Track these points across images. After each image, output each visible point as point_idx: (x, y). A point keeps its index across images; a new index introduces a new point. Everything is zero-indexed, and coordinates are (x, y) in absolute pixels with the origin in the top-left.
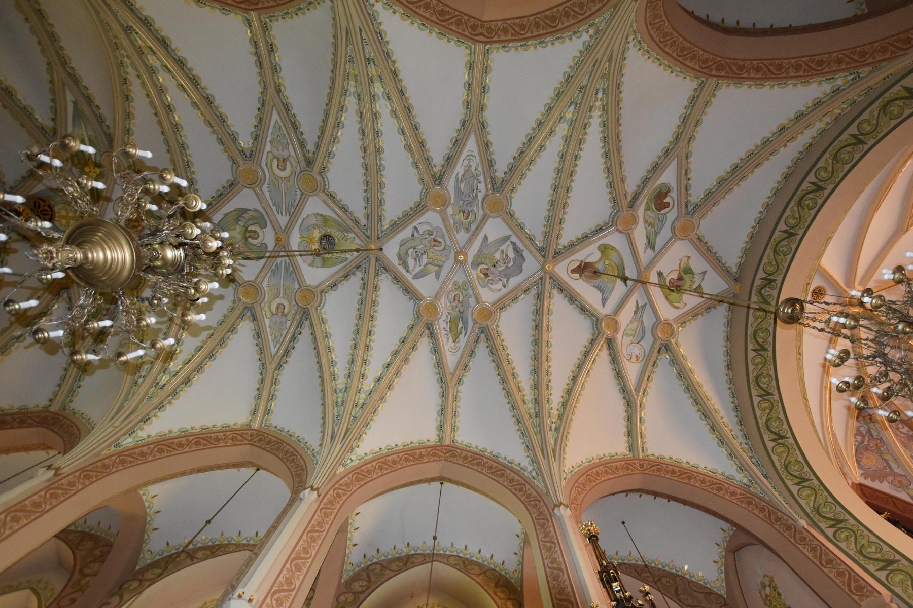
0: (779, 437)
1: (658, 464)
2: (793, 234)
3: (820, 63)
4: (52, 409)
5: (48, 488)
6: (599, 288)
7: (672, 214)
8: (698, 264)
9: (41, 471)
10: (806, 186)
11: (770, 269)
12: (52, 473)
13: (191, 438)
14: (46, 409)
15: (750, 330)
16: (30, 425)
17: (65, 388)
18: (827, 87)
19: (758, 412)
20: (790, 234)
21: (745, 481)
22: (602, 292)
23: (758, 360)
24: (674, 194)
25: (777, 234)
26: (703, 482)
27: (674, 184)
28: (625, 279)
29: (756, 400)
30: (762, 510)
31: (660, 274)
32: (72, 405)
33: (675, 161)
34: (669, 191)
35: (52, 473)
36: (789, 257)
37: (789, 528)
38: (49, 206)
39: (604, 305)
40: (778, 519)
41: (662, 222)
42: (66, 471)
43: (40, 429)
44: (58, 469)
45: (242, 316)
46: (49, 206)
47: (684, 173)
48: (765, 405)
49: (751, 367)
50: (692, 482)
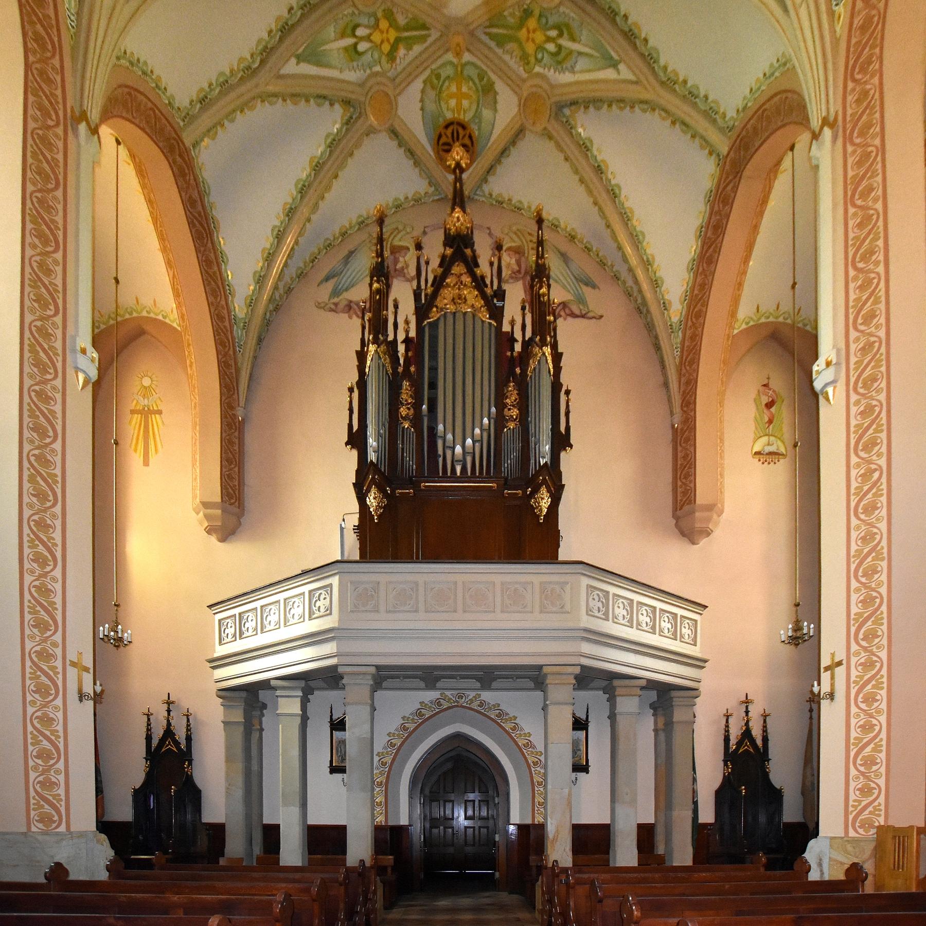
4: (724, 150)
5: (848, 139)
9: (814, 151)
12: (827, 133)
13: (690, 323)
14: (722, 161)
16: (735, 189)
17: (702, 125)
32: (731, 113)
35: (827, 133)
38: (447, 127)
42: (835, 107)
43: (746, 173)
44: (825, 122)
45: (569, 128)
46: (447, 127)
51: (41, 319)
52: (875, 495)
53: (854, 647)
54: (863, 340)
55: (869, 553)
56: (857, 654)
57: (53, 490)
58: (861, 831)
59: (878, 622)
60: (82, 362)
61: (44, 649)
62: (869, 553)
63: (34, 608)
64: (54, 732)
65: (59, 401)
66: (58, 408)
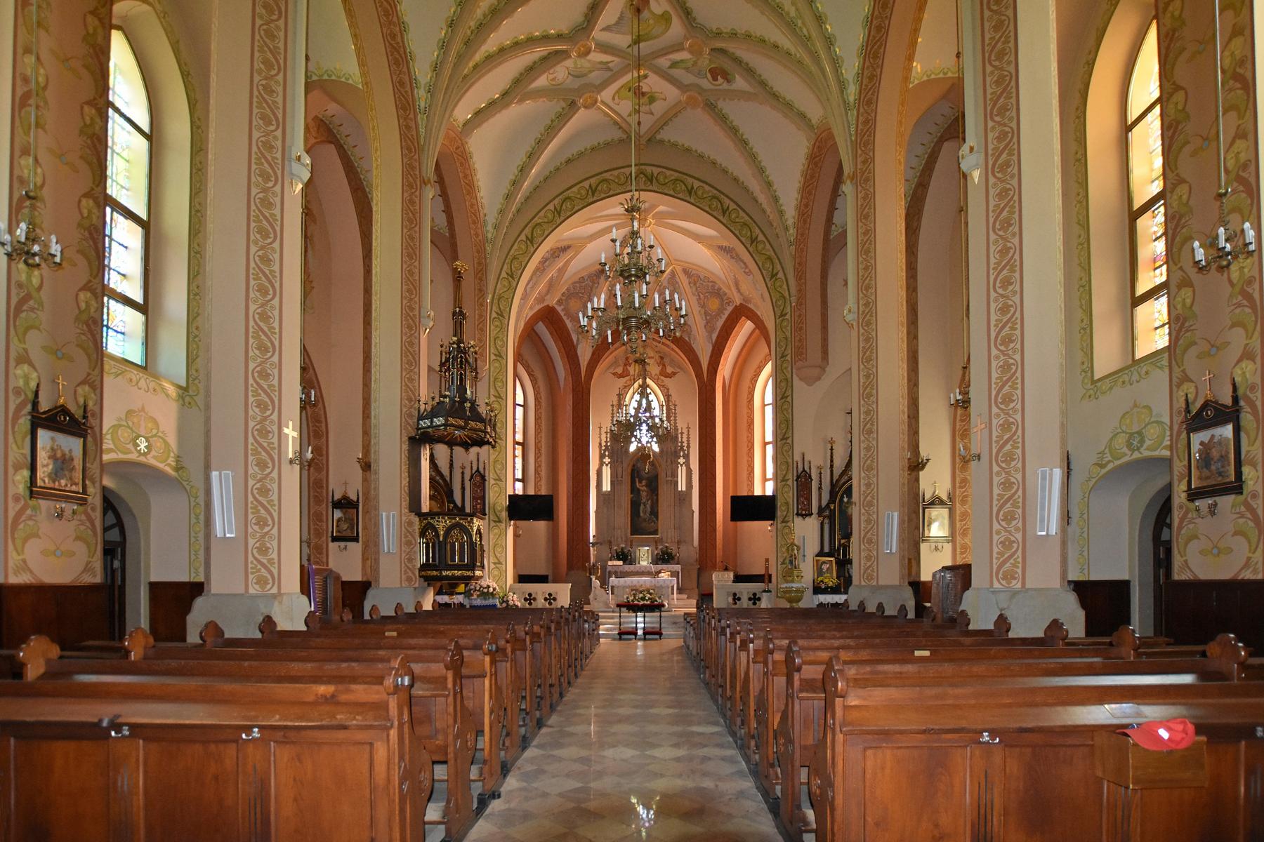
0: (531, 240)
1: (466, 160)
2: (690, 194)
3: (805, 222)
6: (621, 18)
7: (706, 83)
8: (659, 108)
10: (727, 202)
11: (661, 178)
15: (606, 175)
18: (790, 222)
19: (542, 214)
20: (690, 191)
21: (489, 236)
22: (617, 23)
23: (584, 192)
24: (725, 86)
25: (690, 180)
26: (472, 206)
27: (734, 86)
28: (637, 41)
29: (551, 207)
30: (479, 264)
31: (646, 77)
33: (751, 90)
34: (728, 81)
36: (671, 192)
37: (480, 290)
39: (603, 30)
40: (481, 279)
41: (699, 74)
47: (742, 95)
48: (550, 216)
49: (575, 189)
50: (467, 197)
51: (262, 248)
52: (1004, 43)
53: (995, 410)
54: (1000, 186)
55: (1002, 93)
56: (998, 474)
57: (274, 114)
58: (1004, 582)
59: (1013, 387)
60: (296, 167)
61: (262, 528)
62: (1002, 93)
63: (256, 450)
64: (270, 502)
65: (281, 94)
66: (280, 100)
